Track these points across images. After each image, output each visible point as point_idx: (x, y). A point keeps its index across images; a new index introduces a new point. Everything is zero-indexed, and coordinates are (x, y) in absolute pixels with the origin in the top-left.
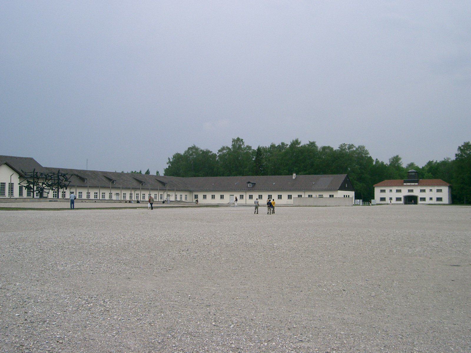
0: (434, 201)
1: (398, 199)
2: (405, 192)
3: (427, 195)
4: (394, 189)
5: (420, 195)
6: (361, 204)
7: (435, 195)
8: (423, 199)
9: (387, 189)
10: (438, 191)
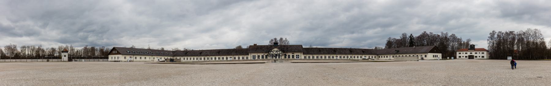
0: (464, 58)
1: (466, 57)
2: (469, 54)
3: (478, 55)
4: (464, 52)
5: (475, 55)
6: (485, 57)
7: (481, 55)
8: (476, 57)
9: (462, 53)
10: (483, 53)
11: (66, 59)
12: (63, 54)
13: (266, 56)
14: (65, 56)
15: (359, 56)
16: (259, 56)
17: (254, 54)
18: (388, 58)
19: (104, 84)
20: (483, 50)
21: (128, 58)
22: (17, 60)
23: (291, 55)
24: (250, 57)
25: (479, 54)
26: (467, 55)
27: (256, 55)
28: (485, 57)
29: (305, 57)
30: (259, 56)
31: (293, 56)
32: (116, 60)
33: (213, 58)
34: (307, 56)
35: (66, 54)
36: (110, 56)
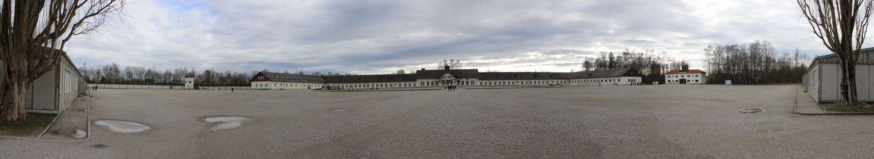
2: (680, 77)
3: (690, 78)
5: (687, 79)
7: (695, 78)
11: (192, 85)
12: (187, 79)
13: (437, 83)
14: (190, 82)
15: (545, 81)
16: (428, 83)
17: (423, 81)
18: (612, 82)
19: (455, 87)
20: (62, 47)
21: (278, 85)
22: (151, 86)
23: (465, 80)
24: (418, 83)
25: (693, 78)
26: (678, 79)
27: (426, 81)
28: (700, 82)
29: (481, 83)
30: (428, 83)
31: (467, 83)
32: (264, 87)
33: (384, 84)
34: (484, 82)
35: (192, 80)
36: (254, 84)
